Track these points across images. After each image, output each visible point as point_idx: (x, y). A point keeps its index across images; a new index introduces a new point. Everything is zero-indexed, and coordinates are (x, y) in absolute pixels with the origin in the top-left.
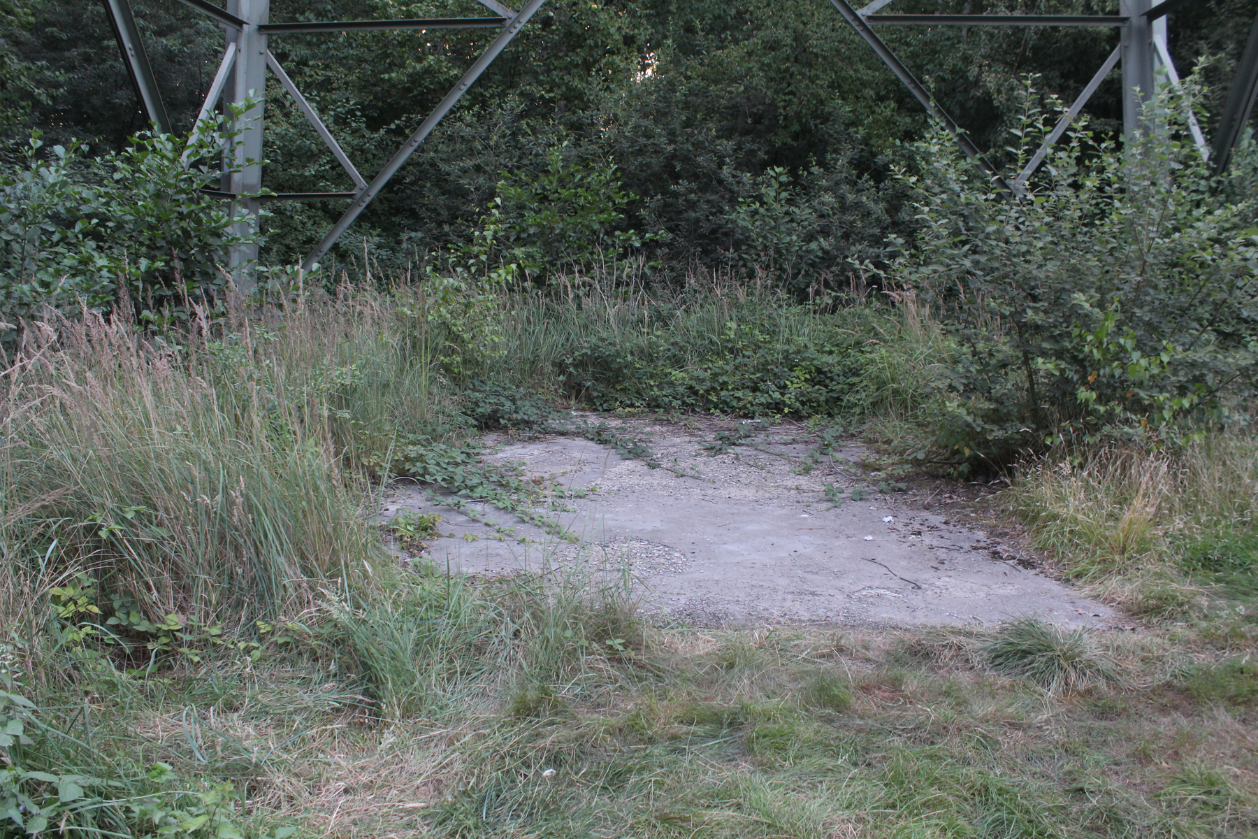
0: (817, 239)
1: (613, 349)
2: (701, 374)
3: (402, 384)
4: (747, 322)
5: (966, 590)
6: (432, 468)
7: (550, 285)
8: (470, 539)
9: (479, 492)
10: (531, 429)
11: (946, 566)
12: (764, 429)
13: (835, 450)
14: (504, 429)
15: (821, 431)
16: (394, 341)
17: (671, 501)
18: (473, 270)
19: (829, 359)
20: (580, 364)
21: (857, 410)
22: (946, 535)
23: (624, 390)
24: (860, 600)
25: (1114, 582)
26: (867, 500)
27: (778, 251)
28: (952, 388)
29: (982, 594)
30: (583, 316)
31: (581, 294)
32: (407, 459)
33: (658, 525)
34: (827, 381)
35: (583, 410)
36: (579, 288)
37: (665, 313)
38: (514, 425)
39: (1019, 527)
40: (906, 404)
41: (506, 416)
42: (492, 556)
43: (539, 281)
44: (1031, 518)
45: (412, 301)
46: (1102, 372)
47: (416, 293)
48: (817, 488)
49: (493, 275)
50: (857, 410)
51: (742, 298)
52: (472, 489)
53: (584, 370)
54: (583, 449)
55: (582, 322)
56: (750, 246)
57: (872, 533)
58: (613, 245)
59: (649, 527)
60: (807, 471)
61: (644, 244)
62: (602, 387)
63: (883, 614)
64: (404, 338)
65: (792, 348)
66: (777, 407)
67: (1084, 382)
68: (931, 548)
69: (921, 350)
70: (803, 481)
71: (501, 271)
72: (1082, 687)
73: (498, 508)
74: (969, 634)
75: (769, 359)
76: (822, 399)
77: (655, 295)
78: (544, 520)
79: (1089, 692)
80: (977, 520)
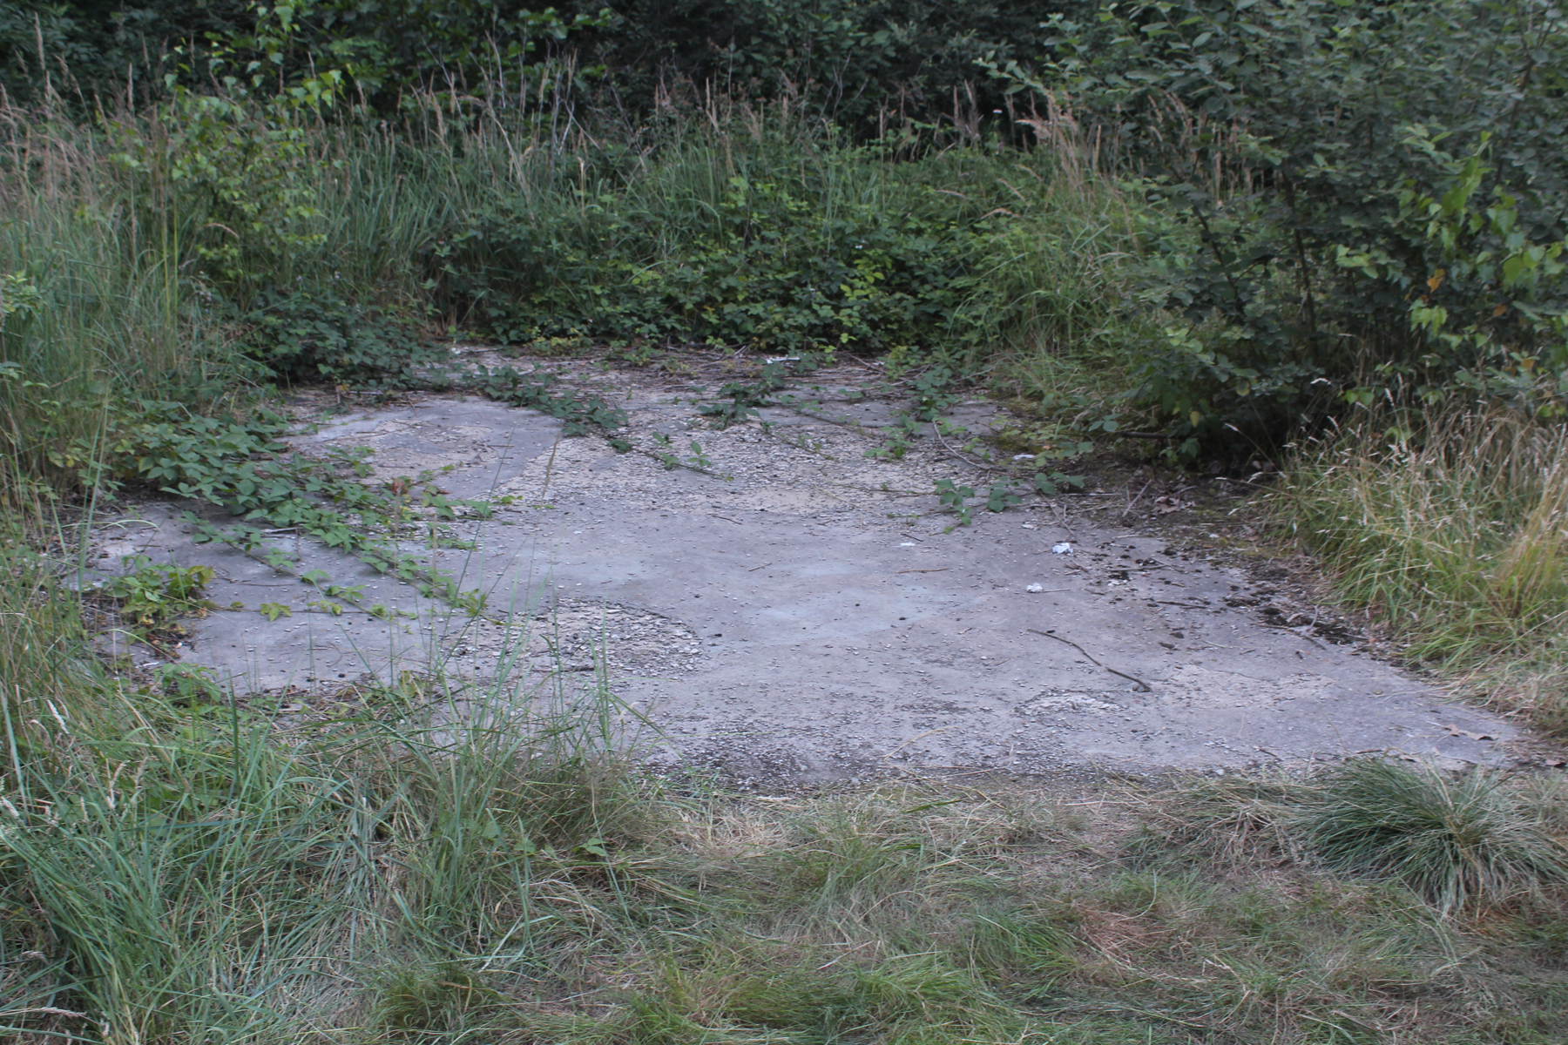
0: (885, 26)
1: (525, 229)
2: (689, 274)
3: (126, 304)
4: (766, 179)
5: (1250, 703)
6: (192, 469)
7: (403, 110)
8: (273, 614)
9: (286, 512)
10: (380, 381)
11: (1187, 642)
12: (808, 373)
13: (942, 413)
14: (327, 383)
15: (910, 375)
16: (108, 219)
17: (654, 521)
18: (257, 81)
19: (920, 244)
20: (463, 257)
21: (973, 337)
22: (1175, 578)
23: (549, 305)
24: (1041, 718)
25: (1505, 671)
26: (1015, 510)
27: (818, 48)
28: (1172, 302)
29: (1266, 700)
30: (467, 167)
31: (461, 126)
32: (142, 451)
33: (636, 569)
34: (915, 284)
35: (473, 342)
36: (457, 115)
37: (617, 162)
38: (345, 376)
39: (1305, 561)
40: (1066, 326)
41: (331, 359)
42: (320, 648)
43: (383, 103)
44: (1330, 544)
45: (139, 141)
46: (1455, 272)
47: (147, 126)
48: (921, 487)
49: (295, 91)
50: (973, 337)
51: (756, 130)
52: (272, 507)
53: (472, 269)
54: (477, 419)
55: (465, 181)
56: (766, 38)
57: (1038, 577)
58: (517, 37)
59: (620, 577)
60: (897, 454)
61: (571, 34)
62: (505, 300)
63: (1090, 747)
64: (126, 214)
65: (851, 225)
66: (828, 332)
67: (1420, 290)
68: (1152, 604)
69: (1087, 226)
70: (893, 474)
71: (311, 84)
72: (1500, 896)
73: (325, 546)
74: (1270, 794)
75: (809, 244)
76: (908, 316)
77: (595, 131)
78: (419, 567)
79: (1514, 905)
80: (1223, 546)
